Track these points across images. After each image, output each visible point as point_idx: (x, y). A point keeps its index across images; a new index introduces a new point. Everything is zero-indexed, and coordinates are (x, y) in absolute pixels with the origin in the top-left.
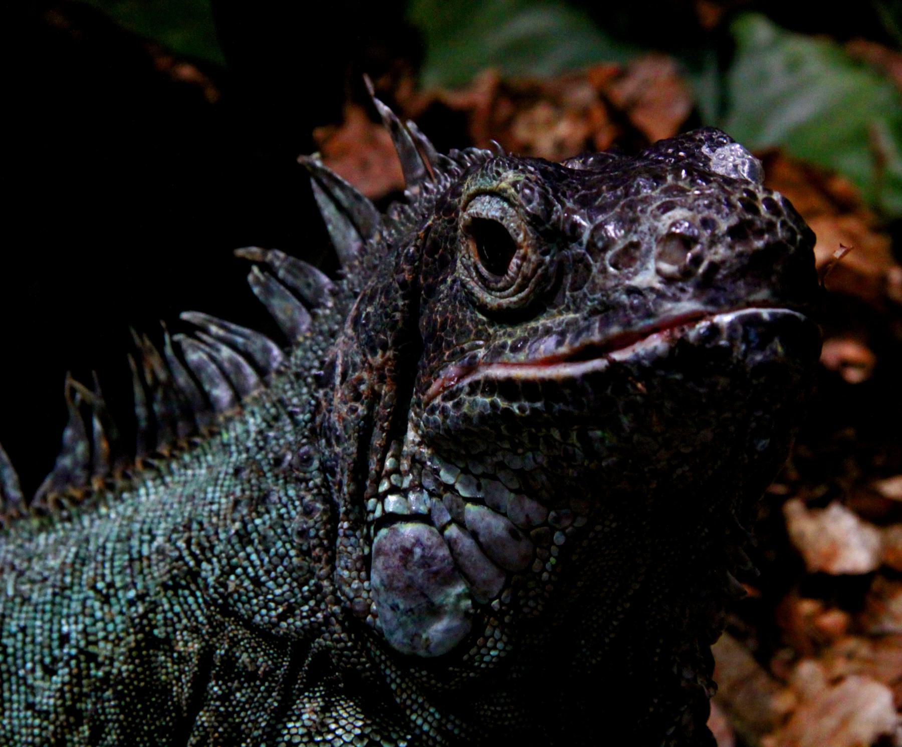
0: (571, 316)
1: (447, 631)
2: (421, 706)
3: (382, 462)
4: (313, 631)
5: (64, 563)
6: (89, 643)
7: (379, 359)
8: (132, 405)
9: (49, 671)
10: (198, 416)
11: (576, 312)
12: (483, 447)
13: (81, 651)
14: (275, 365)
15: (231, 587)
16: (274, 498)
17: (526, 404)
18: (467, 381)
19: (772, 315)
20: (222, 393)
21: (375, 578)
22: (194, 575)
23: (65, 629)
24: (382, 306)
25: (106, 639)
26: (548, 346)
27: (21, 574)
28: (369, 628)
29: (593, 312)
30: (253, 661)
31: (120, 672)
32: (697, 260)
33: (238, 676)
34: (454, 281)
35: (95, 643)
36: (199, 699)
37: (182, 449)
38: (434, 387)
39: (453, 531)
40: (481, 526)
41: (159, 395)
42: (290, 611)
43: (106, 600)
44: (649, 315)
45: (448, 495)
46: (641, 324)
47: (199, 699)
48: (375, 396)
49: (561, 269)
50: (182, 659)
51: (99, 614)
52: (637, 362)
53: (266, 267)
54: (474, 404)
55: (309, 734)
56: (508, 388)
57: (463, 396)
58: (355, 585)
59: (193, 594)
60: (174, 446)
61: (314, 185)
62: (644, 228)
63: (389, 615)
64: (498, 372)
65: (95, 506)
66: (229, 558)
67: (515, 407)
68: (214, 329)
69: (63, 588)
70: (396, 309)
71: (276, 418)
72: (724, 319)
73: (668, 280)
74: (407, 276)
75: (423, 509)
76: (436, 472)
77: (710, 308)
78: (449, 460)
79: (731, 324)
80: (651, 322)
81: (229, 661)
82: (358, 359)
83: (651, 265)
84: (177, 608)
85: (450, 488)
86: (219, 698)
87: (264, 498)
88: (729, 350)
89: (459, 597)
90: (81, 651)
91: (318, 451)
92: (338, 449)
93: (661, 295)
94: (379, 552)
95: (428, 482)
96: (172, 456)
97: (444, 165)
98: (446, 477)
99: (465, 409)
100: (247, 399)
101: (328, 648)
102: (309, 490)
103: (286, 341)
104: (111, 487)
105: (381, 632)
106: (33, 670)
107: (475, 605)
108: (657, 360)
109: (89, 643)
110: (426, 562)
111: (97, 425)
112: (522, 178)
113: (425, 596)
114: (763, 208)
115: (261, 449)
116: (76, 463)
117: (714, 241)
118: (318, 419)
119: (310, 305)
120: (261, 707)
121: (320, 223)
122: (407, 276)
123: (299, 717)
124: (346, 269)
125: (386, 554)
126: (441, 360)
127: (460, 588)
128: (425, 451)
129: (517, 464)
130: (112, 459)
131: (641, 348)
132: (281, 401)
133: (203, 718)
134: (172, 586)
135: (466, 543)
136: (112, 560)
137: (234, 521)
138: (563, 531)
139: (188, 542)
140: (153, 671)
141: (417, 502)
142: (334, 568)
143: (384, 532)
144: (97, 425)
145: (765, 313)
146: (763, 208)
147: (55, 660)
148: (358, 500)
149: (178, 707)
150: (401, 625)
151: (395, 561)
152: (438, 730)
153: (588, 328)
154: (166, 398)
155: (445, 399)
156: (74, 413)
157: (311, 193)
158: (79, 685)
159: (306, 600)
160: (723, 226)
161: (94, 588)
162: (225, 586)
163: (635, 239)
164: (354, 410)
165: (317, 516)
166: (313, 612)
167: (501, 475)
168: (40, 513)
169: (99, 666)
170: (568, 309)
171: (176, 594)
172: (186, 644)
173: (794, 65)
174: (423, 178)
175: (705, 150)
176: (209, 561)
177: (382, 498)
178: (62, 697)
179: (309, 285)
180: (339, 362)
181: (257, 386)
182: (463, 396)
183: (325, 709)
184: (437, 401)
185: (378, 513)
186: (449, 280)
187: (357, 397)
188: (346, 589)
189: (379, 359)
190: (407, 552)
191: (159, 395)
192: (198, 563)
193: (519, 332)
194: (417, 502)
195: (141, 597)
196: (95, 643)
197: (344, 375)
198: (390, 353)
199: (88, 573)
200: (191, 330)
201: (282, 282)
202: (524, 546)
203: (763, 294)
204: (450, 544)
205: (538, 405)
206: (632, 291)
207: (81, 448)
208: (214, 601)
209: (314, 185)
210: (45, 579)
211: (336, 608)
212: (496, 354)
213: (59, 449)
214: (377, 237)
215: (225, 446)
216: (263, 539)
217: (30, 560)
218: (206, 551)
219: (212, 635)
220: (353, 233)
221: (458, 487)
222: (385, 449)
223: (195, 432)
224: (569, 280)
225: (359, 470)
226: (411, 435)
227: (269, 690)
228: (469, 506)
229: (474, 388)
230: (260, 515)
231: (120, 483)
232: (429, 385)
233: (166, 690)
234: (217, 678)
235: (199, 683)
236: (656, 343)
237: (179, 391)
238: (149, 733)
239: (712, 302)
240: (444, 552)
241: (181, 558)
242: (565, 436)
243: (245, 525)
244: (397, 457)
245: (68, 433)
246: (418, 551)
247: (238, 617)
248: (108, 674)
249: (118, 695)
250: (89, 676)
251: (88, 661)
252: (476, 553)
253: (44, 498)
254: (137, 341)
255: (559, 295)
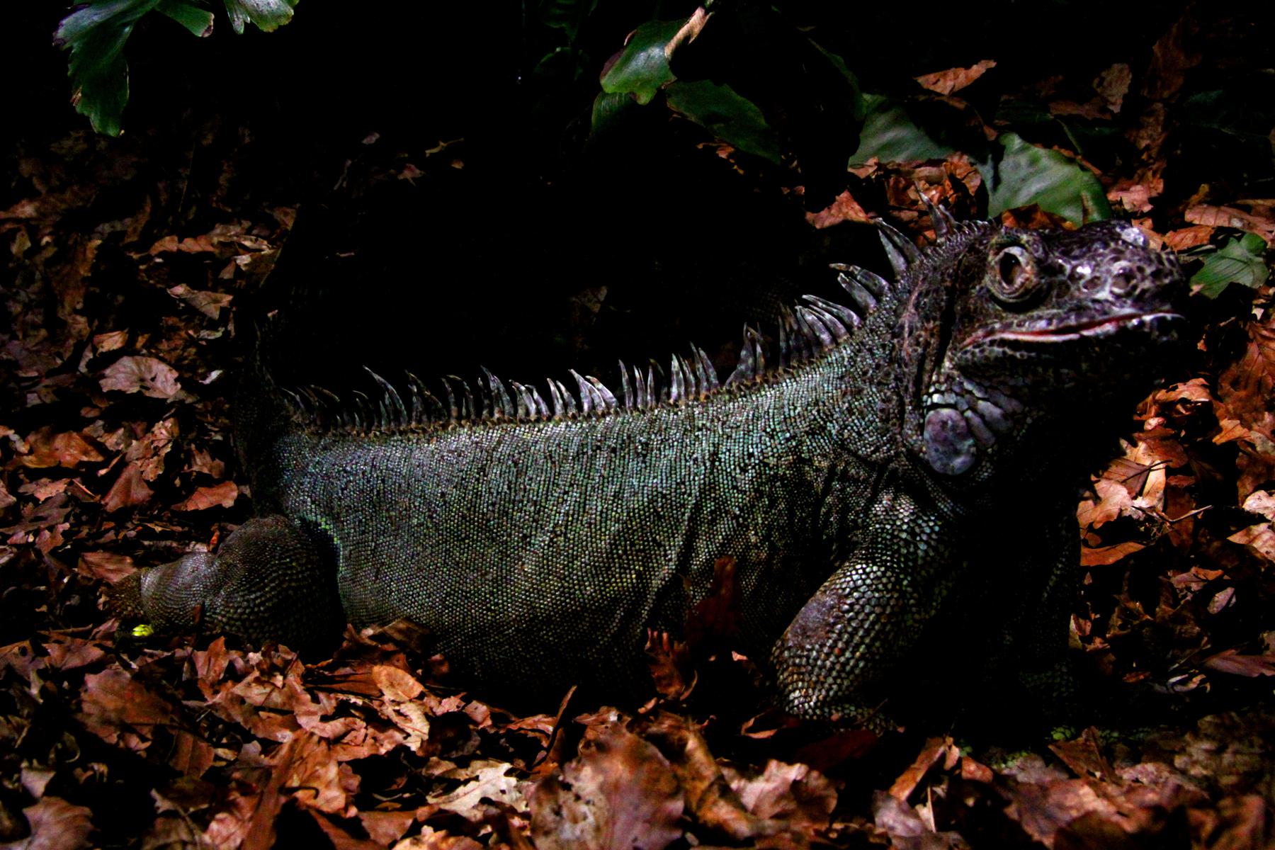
0: (1055, 311)
1: (964, 462)
2: (944, 499)
3: (930, 377)
4: (889, 460)
5: (747, 419)
6: (764, 458)
7: (931, 325)
8: (779, 341)
9: (744, 470)
10: (814, 349)
11: (1060, 308)
12: (993, 372)
13: (760, 461)
14: (856, 324)
15: (846, 436)
16: (865, 392)
17: (1025, 354)
18: (988, 339)
19: (1173, 318)
20: (825, 337)
21: (926, 435)
22: (823, 428)
23: (751, 450)
24: (935, 299)
25: (773, 456)
26: (1042, 324)
27: (724, 423)
28: (921, 460)
29: (1071, 310)
30: (858, 473)
31: (785, 474)
32: (1135, 287)
33: (848, 480)
34: (982, 288)
35: (768, 458)
36: (827, 490)
37: (805, 364)
38: (968, 340)
39: (969, 414)
40: (986, 413)
41: (793, 337)
42: (877, 450)
43: (772, 437)
44: (1105, 313)
45: (967, 396)
46: (1099, 318)
47: (827, 490)
48: (927, 344)
49: (1050, 286)
50: (818, 470)
51: (768, 444)
52: (1097, 337)
53: (847, 274)
54: (991, 351)
55: (886, 511)
56: (1015, 345)
57: (985, 347)
58: (915, 438)
59: (823, 438)
60: (800, 362)
61: (881, 234)
62: (1103, 269)
63: (933, 453)
64: (1011, 337)
65: (759, 391)
66: (844, 421)
67: (1018, 355)
68: (820, 304)
69: (749, 431)
70: (942, 300)
71: (859, 351)
72: (1148, 318)
73: (1118, 297)
74: (948, 284)
75: (952, 401)
76: (961, 384)
77: (1141, 312)
78: (970, 380)
79: (1152, 321)
80: (1106, 317)
81: (845, 471)
82: (919, 325)
83: (1107, 288)
84: (814, 444)
85: (970, 392)
86: (839, 490)
87: (860, 391)
88: (1149, 334)
89: (970, 446)
90: (760, 461)
91: (893, 369)
92: (906, 370)
93: (1113, 304)
94: (929, 422)
95: (956, 389)
96: (799, 367)
97: (960, 228)
98: (968, 386)
99: (986, 353)
100: (840, 340)
101: (897, 469)
102: (889, 389)
103: (862, 311)
104: (767, 381)
105: (928, 462)
106: (735, 469)
107: (978, 450)
108: (1108, 336)
109: (764, 458)
110: (954, 428)
111: (759, 349)
112: (1031, 238)
113: (952, 444)
114: (1166, 263)
115: (852, 366)
116: (747, 369)
117: (1143, 279)
118: (894, 354)
119: (877, 296)
120: (861, 495)
121: (884, 254)
122: (948, 284)
123: (881, 502)
124: (899, 277)
125: (933, 424)
126: (973, 327)
127: (971, 442)
128: (956, 373)
129: (1012, 383)
130: (766, 367)
131: (1099, 330)
132: (862, 343)
133: (829, 499)
134: (811, 433)
135: (976, 420)
136: (773, 418)
137: (844, 403)
138: (1032, 417)
139: (818, 411)
140: (803, 475)
141: (951, 399)
142: (902, 429)
143: (932, 412)
144: (759, 349)
145: (1169, 316)
146: (1166, 263)
147: (746, 465)
148: (917, 396)
149: (817, 493)
150: (940, 459)
151: (938, 427)
152: (952, 511)
153: (1068, 318)
154: (796, 339)
155: (975, 347)
156: (747, 342)
157: (879, 238)
158: (761, 478)
159: (885, 444)
160: (1148, 271)
161: (765, 431)
162: (842, 435)
163: (1098, 274)
164: (916, 351)
165: (894, 403)
166: (889, 450)
167: (1001, 387)
168: (729, 392)
169: (770, 469)
170: (1053, 307)
171: (813, 437)
172: (820, 462)
173: (1033, 162)
174: (946, 234)
175: (1118, 230)
176: (831, 422)
177: (930, 395)
178: (753, 484)
179: (875, 285)
180: (906, 325)
181: (845, 334)
182: (985, 347)
183: (894, 499)
184: (969, 348)
185: (929, 403)
186: (978, 287)
187: (918, 344)
188: (910, 440)
189: (931, 325)
190: (944, 423)
191: (793, 337)
192: (825, 423)
193: (1022, 317)
194: (951, 399)
195: (793, 437)
196: (768, 458)
197: (910, 333)
198: (938, 323)
199: (761, 424)
200: (806, 304)
201: (859, 282)
202: (1010, 423)
203: (1167, 307)
204: (967, 420)
205: (1033, 354)
206: (1095, 301)
207: (750, 361)
208: (836, 442)
209: (881, 234)
210: (739, 427)
211: (903, 449)
212: (1007, 327)
213: (738, 360)
214: (918, 262)
215: (830, 364)
216: (861, 413)
217: (727, 416)
218: (829, 417)
219: (835, 459)
220: (902, 260)
221: (975, 392)
222: (932, 371)
223: (812, 355)
224: (1055, 293)
225: (918, 381)
226: (947, 364)
227: (866, 488)
228: (980, 402)
229: (992, 343)
230: (857, 400)
231: (771, 380)
232: (964, 339)
233: (810, 484)
234: (838, 480)
235: (828, 482)
236: (1109, 328)
237: (804, 335)
238: (801, 505)
239: (1141, 309)
240: (963, 423)
241: (815, 419)
242: (1045, 371)
243: (850, 405)
244: (939, 374)
245: (743, 353)
246: (950, 422)
247: (849, 451)
248: (776, 474)
249: (783, 485)
250: (765, 474)
251: (764, 467)
252: (982, 426)
253: (730, 384)
254: (783, 310)
255: (1048, 300)
